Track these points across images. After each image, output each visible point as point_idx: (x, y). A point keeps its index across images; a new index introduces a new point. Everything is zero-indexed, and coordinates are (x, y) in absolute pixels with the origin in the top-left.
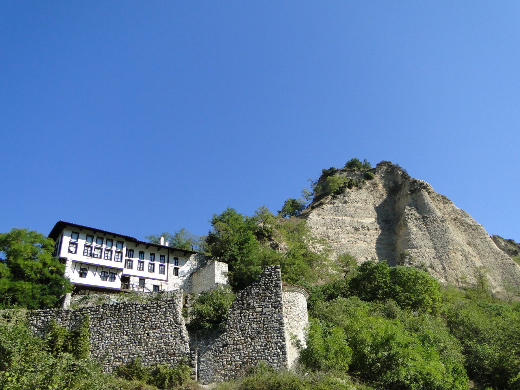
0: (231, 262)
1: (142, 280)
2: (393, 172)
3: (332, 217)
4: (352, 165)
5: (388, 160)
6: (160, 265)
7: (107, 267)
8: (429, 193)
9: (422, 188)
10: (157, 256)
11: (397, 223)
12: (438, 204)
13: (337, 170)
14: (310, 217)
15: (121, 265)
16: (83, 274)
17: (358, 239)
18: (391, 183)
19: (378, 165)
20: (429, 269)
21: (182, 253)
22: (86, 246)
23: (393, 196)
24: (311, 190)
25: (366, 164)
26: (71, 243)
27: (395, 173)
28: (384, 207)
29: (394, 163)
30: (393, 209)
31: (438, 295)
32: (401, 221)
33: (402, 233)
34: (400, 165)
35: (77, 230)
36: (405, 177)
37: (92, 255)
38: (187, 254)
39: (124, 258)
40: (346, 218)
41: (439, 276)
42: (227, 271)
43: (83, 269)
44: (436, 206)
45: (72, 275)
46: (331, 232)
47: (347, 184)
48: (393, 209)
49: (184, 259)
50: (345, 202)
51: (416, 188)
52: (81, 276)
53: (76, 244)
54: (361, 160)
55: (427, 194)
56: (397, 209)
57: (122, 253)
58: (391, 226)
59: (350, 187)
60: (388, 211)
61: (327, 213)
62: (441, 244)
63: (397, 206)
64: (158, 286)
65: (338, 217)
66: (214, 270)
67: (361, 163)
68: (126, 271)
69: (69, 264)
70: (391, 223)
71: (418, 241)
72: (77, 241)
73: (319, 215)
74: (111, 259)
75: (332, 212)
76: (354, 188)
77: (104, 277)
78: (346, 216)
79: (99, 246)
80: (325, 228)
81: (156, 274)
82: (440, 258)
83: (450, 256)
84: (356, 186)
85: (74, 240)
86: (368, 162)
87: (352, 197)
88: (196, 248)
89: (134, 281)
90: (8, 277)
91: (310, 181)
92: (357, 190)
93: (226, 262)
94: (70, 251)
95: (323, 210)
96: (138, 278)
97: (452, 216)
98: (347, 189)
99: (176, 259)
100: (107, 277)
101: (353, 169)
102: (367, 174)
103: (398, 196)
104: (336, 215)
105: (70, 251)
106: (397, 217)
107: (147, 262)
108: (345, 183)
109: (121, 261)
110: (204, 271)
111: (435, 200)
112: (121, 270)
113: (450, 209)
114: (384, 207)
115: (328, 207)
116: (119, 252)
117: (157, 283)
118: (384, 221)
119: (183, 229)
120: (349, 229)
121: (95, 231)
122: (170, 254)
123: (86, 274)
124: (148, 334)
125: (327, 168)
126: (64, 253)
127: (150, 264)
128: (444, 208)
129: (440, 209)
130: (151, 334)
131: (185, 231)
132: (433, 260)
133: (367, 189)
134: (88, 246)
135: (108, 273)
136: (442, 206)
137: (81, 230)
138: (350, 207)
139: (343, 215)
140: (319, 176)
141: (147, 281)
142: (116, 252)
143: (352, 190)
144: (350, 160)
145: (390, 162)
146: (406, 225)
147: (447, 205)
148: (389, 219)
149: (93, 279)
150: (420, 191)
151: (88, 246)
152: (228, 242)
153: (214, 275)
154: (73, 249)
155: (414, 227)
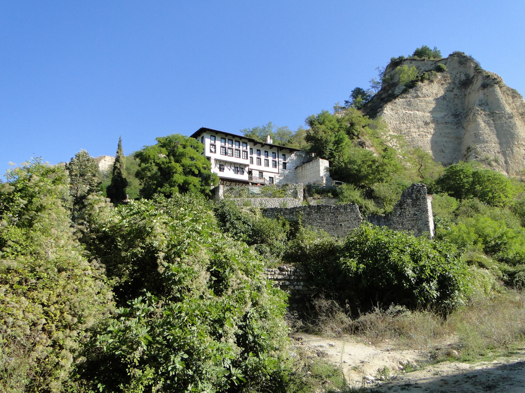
0: (330, 158)
1: (261, 172)
2: (466, 64)
3: (404, 112)
4: (420, 53)
5: (461, 51)
6: (265, 159)
7: (237, 164)
8: (501, 87)
9: (495, 83)
10: (270, 153)
11: (465, 117)
12: (507, 99)
13: (407, 59)
14: (385, 112)
15: (247, 162)
16: (221, 169)
17: (428, 133)
18: (463, 75)
19: (450, 55)
20: (494, 164)
21: (288, 151)
22: (221, 147)
23: (464, 90)
24: (378, 79)
25: (436, 52)
26: (211, 145)
27: (468, 65)
28: (454, 101)
29: (467, 54)
30: (462, 103)
31: (483, 173)
32: (471, 116)
33: (471, 127)
34: (473, 57)
35: (215, 134)
36: (478, 70)
37: (226, 154)
38: (292, 151)
39: (249, 156)
40: (417, 112)
41: (501, 169)
42: (328, 166)
43: (222, 165)
44: (506, 101)
45: (215, 169)
46: (404, 126)
47: (420, 78)
48: (462, 103)
49: (289, 155)
50: (418, 96)
51: (489, 82)
52: (220, 171)
53: (215, 146)
54: (432, 48)
55: (499, 88)
56: (466, 104)
57: (247, 152)
58: (459, 120)
59: (422, 81)
60: (457, 105)
61: (400, 107)
62: (506, 137)
63: (466, 100)
64: (273, 178)
65: (410, 112)
66: (319, 166)
67: (431, 50)
68: (251, 166)
69: (213, 161)
70: (460, 118)
71: (485, 136)
72: (215, 143)
73: (392, 110)
74: (233, 156)
75: (405, 106)
76: (426, 82)
77: (236, 171)
78: (418, 110)
79: (237, 147)
80: (398, 123)
81: (271, 168)
82: (504, 154)
83: (514, 151)
84: (429, 79)
85: (213, 142)
86: (438, 50)
87: (424, 91)
88: (295, 145)
89: (255, 174)
90: (176, 173)
91: (377, 71)
92: (429, 84)
93: (327, 159)
94: (211, 151)
95: (395, 105)
96: (258, 172)
97: (520, 111)
98: (420, 83)
99: (284, 155)
100: (238, 171)
101: (423, 58)
102: (439, 66)
103: (468, 90)
104: (408, 110)
105: (211, 151)
106: (465, 111)
107: (263, 157)
108: (417, 77)
109: (247, 158)
110: (309, 166)
111: (505, 94)
112: (248, 165)
113: (518, 104)
114: (454, 101)
115: (400, 102)
116: (245, 151)
117: (272, 175)
118: (452, 115)
119: (270, 123)
120: (420, 123)
121: (227, 134)
122: (279, 152)
123: (224, 169)
124: (341, 225)
125: (396, 57)
126: (208, 154)
127: (265, 159)
128: (513, 102)
129: (509, 104)
130: (343, 225)
131: (272, 125)
132: (497, 154)
133: (438, 82)
134: (223, 147)
135: (239, 168)
136: (511, 100)
137: (217, 134)
138: (421, 101)
139: (414, 110)
140: (387, 65)
141: (264, 173)
142: (243, 151)
143: (424, 84)
144: (420, 47)
145: (463, 53)
146: (475, 121)
147: (516, 99)
148: (458, 113)
149: (229, 173)
150: (492, 86)
151: (223, 147)
152: (326, 142)
153: (319, 170)
154: (213, 150)
155: (482, 123)
